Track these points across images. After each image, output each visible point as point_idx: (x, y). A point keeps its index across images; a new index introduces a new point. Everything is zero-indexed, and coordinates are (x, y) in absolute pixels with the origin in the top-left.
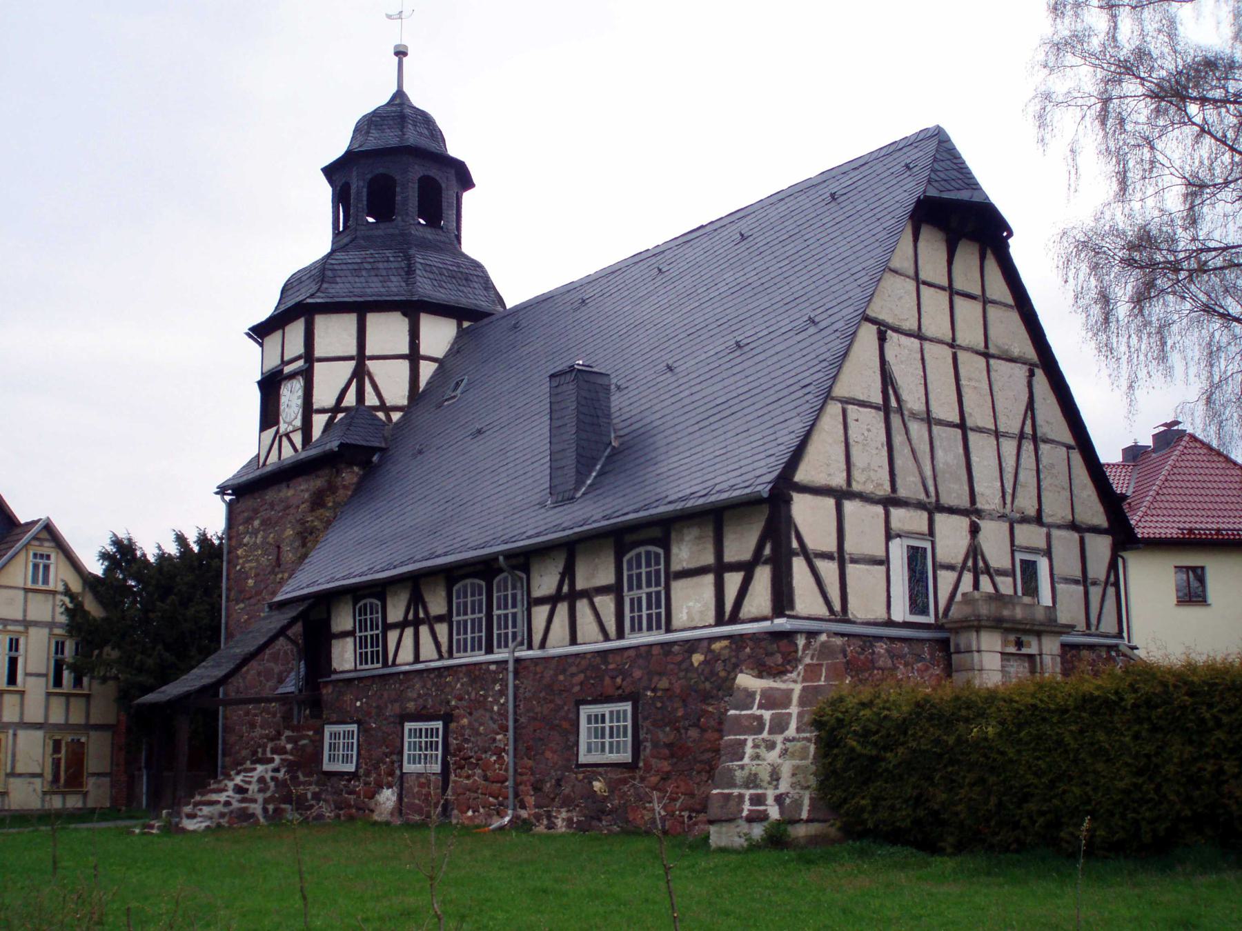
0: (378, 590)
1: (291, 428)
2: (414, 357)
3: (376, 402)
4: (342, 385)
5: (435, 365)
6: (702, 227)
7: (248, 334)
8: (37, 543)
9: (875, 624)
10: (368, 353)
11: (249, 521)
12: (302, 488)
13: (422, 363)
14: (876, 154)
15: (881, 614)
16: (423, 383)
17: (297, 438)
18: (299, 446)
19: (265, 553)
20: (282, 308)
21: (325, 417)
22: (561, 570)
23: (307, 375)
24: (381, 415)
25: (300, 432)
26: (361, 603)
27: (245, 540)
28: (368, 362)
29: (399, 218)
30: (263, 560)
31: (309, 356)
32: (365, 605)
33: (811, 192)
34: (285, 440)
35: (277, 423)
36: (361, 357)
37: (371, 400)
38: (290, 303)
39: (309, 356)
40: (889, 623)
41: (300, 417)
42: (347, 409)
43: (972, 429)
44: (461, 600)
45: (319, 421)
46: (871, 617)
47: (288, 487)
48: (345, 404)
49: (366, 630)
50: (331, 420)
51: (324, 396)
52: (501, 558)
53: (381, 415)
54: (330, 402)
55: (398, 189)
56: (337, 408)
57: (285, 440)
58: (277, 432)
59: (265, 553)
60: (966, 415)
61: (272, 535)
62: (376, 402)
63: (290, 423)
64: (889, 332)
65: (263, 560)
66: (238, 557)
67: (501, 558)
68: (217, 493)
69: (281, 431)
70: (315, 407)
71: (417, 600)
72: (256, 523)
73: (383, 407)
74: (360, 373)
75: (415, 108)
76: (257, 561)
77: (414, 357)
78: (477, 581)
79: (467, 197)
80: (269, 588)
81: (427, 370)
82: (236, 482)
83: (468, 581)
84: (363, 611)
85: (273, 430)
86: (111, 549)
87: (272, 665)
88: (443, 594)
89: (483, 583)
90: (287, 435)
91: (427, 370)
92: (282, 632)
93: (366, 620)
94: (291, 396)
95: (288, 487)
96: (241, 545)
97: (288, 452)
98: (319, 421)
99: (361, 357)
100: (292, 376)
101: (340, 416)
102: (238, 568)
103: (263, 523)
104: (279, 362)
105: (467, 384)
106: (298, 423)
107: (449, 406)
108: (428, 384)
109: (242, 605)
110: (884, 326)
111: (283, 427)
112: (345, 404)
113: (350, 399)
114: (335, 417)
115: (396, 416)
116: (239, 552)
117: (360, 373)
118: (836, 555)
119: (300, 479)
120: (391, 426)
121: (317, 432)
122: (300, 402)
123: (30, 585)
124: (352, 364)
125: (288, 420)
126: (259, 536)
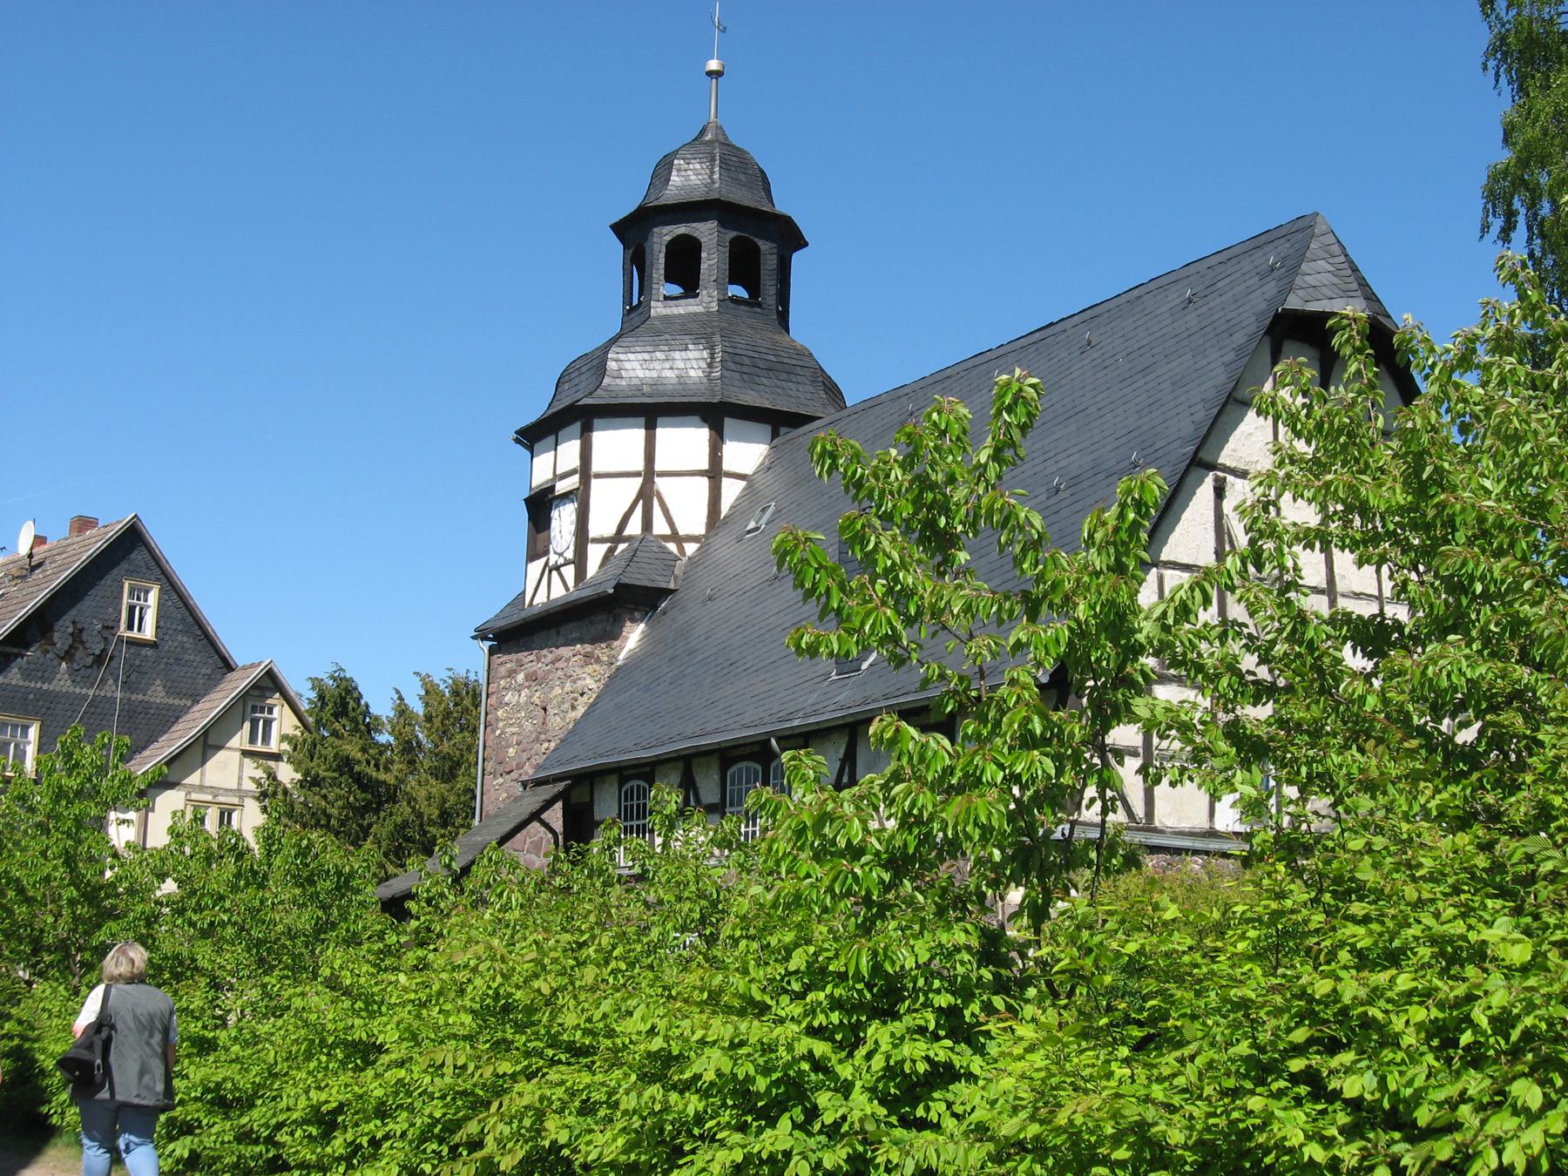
0: (647, 771)
1: (561, 561)
2: (715, 473)
3: (668, 531)
4: (626, 508)
5: (743, 484)
6: (1052, 324)
7: (517, 441)
8: (257, 693)
9: (1192, 834)
10: (658, 467)
11: (511, 674)
12: (573, 636)
13: (726, 482)
14: (1290, 226)
15: (1201, 822)
16: (725, 507)
17: (569, 572)
18: (571, 583)
19: (529, 717)
20: (550, 412)
21: (605, 547)
22: (841, 756)
23: (581, 497)
24: (672, 547)
25: (572, 567)
26: (627, 786)
27: (506, 699)
28: (657, 480)
29: (705, 292)
30: (528, 726)
31: (585, 470)
32: (632, 788)
33: (1257, 255)
34: (554, 573)
35: (546, 553)
36: (649, 473)
37: (660, 527)
38: (559, 406)
39: (585, 470)
40: (1212, 834)
41: (572, 548)
42: (629, 539)
43: (1343, 595)
44: (736, 788)
45: (595, 553)
46: (1185, 825)
47: (558, 633)
48: (627, 532)
49: (632, 819)
50: (611, 551)
51: (602, 523)
52: (773, 741)
53: (672, 547)
54: (610, 531)
55: (704, 255)
56: (618, 537)
57: (554, 573)
58: (547, 564)
59: (529, 717)
60: (1337, 578)
61: (538, 694)
62: (668, 531)
63: (561, 555)
64: (1230, 478)
65: (528, 726)
66: (498, 720)
67: (773, 741)
68: (474, 638)
69: (551, 563)
70: (591, 535)
71: (688, 785)
72: (520, 677)
73: (675, 537)
74: (647, 495)
75: (734, 146)
76: (520, 725)
77: (715, 473)
78: (753, 765)
79: (797, 258)
80: (532, 760)
81: (731, 491)
82: (502, 623)
83: (743, 765)
84: (629, 795)
85: (541, 562)
86: (486, 645)
87: (533, 857)
88: (716, 777)
89: (759, 768)
90: (557, 568)
91: (731, 491)
92: (536, 816)
93: (632, 806)
94: (563, 520)
95: (558, 633)
96: (501, 704)
97: (558, 591)
98: (595, 553)
99: (649, 473)
100: (567, 496)
101: (622, 547)
102: (498, 732)
103: (527, 678)
104: (551, 476)
105: (774, 513)
106: (570, 555)
107: (750, 539)
108: (732, 507)
109: (501, 780)
110: (1223, 471)
111: (553, 559)
112: (627, 532)
113: (634, 527)
114: (616, 548)
115: (691, 548)
116: (499, 713)
117: (647, 495)
118: (1141, 751)
119: (571, 625)
120: (685, 559)
121: (592, 568)
122: (572, 528)
123: (248, 747)
124: (639, 481)
125: (559, 551)
126: (523, 694)
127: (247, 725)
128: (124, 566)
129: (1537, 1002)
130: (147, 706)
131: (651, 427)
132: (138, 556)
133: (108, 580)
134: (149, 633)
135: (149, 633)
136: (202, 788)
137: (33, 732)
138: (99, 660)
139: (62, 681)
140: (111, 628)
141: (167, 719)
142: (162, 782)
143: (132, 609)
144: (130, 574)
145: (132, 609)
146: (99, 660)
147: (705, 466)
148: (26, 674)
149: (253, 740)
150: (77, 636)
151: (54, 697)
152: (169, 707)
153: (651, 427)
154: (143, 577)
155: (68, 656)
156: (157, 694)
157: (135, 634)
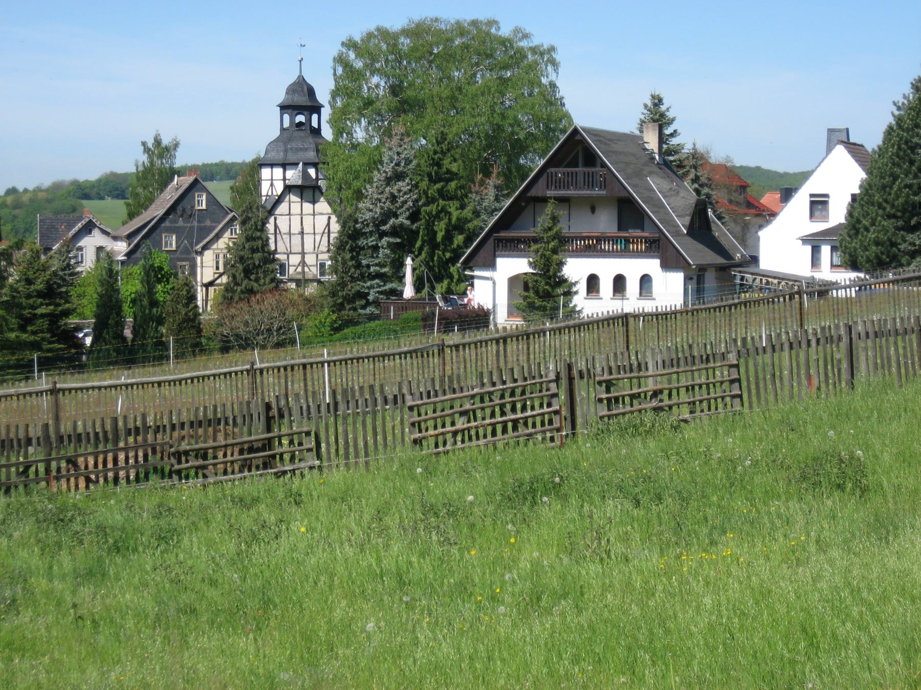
36: (272, 180)
74: (272, 185)
99: (272, 180)
113: (270, 193)
117: (272, 185)
127: (229, 230)
128: (195, 189)
129: (155, 310)
130: (205, 227)
131: (272, 168)
132: (198, 186)
133: (190, 194)
134: (204, 207)
135: (204, 207)
136: (218, 249)
137: (174, 237)
138: (190, 216)
139: (181, 223)
140: (193, 207)
141: (211, 229)
142: (205, 248)
143: (199, 201)
144: (197, 191)
145: (199, 201)
146: (190, 216)
147: (282, 178)
148: (171, 222)
149: (232, 234)
150: (184, 210)
151: (179, 228)
152: (212, 226)
153: (272, 168)
154: (200, 192)
155: (182, 216)
156: (208, 223)
157: (200, 208)
